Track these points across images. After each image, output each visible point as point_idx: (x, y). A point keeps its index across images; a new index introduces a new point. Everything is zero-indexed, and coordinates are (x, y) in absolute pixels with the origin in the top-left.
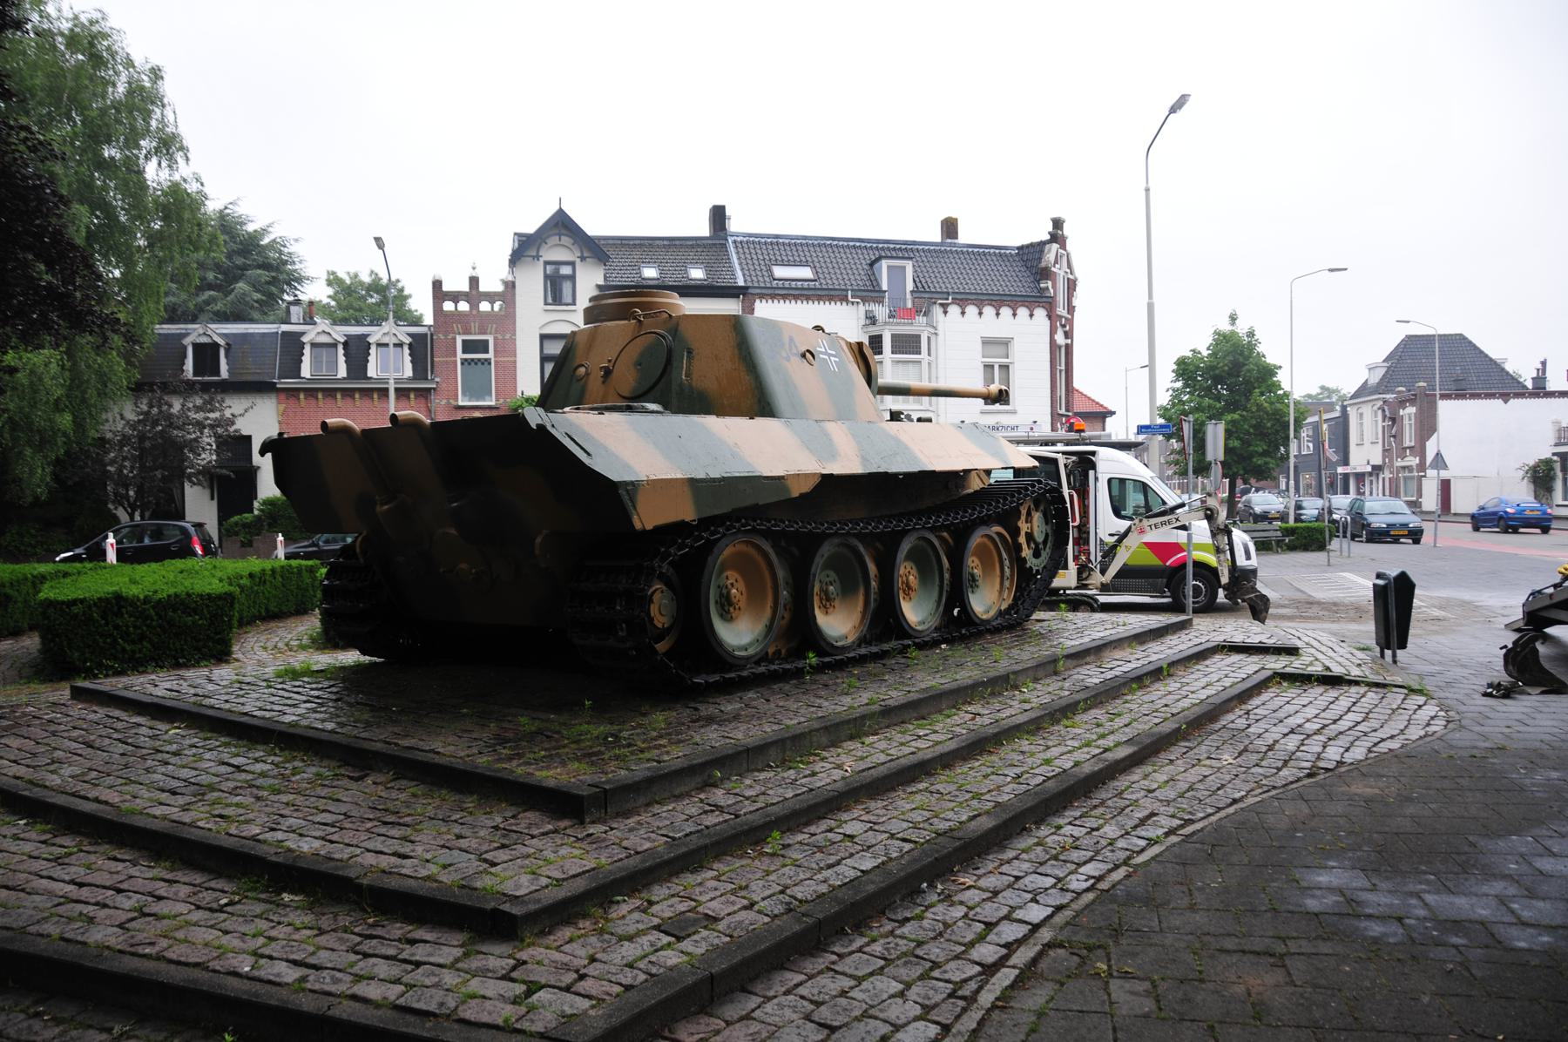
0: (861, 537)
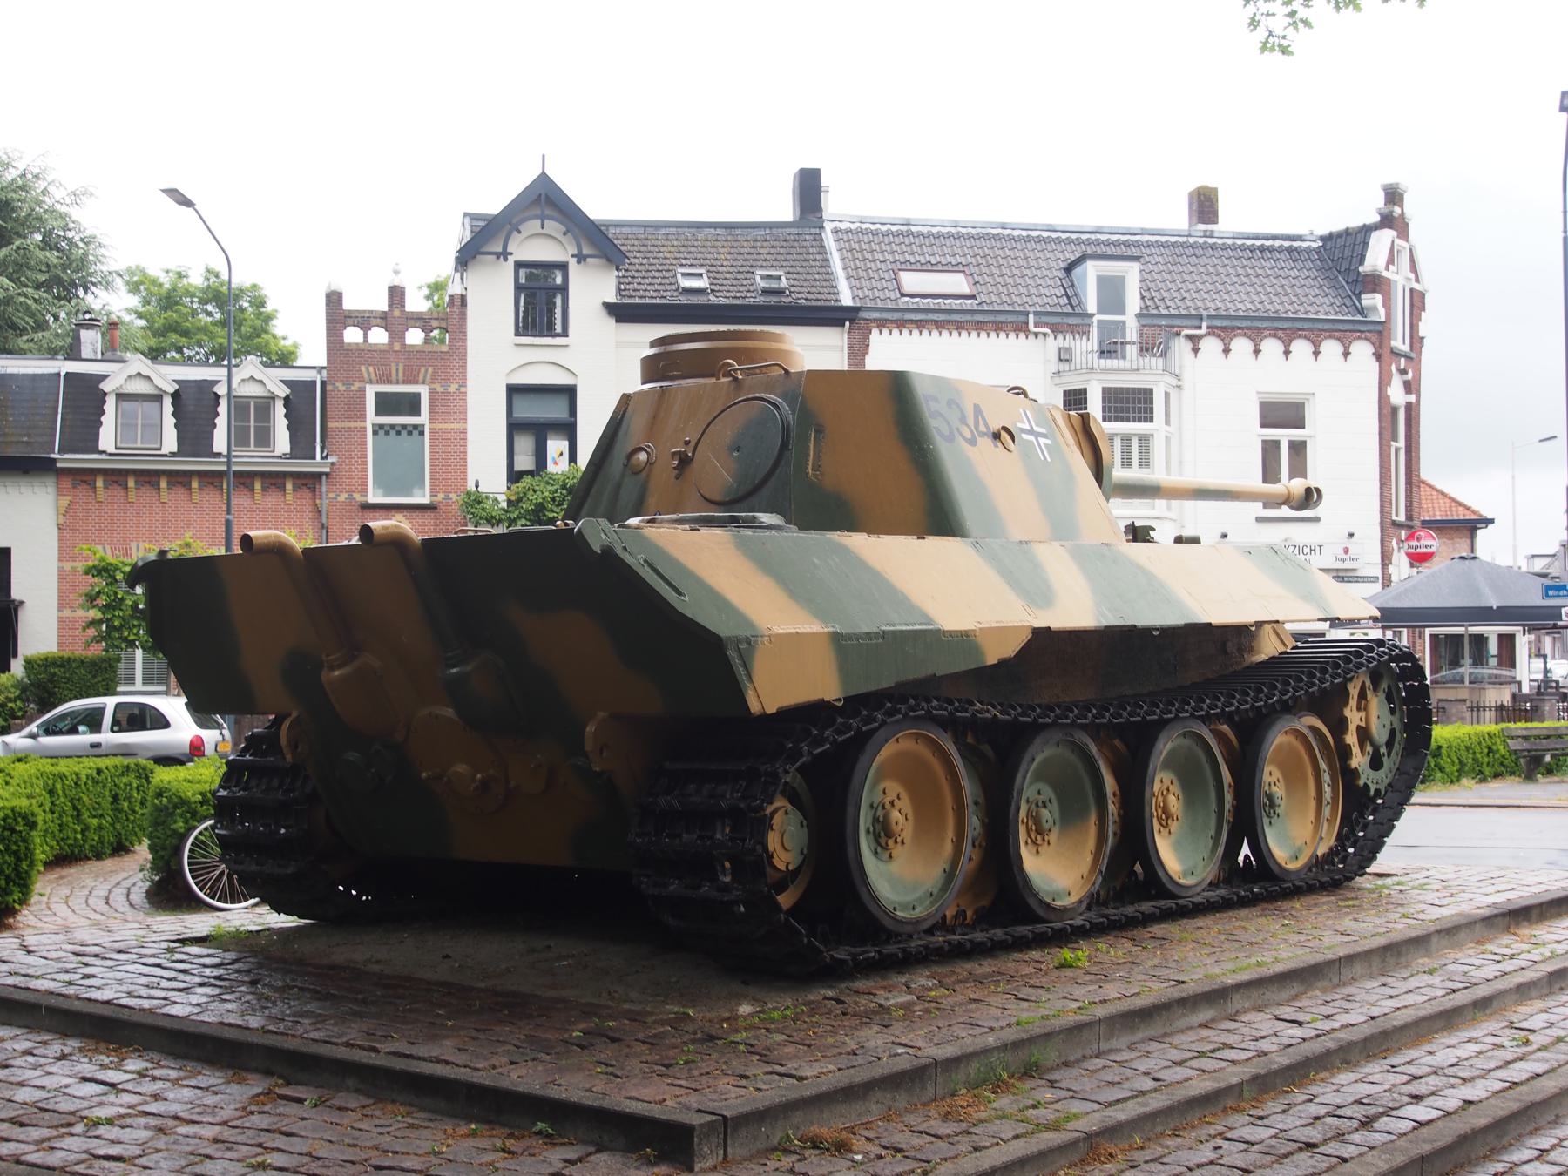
0: (1094, 731)
